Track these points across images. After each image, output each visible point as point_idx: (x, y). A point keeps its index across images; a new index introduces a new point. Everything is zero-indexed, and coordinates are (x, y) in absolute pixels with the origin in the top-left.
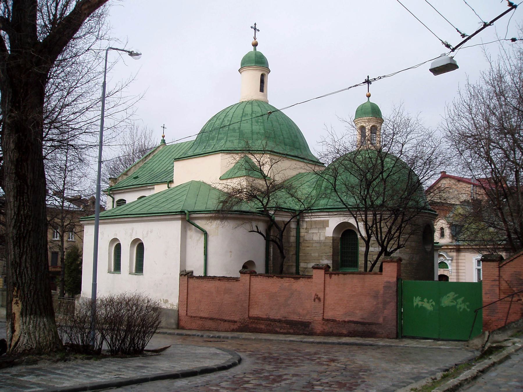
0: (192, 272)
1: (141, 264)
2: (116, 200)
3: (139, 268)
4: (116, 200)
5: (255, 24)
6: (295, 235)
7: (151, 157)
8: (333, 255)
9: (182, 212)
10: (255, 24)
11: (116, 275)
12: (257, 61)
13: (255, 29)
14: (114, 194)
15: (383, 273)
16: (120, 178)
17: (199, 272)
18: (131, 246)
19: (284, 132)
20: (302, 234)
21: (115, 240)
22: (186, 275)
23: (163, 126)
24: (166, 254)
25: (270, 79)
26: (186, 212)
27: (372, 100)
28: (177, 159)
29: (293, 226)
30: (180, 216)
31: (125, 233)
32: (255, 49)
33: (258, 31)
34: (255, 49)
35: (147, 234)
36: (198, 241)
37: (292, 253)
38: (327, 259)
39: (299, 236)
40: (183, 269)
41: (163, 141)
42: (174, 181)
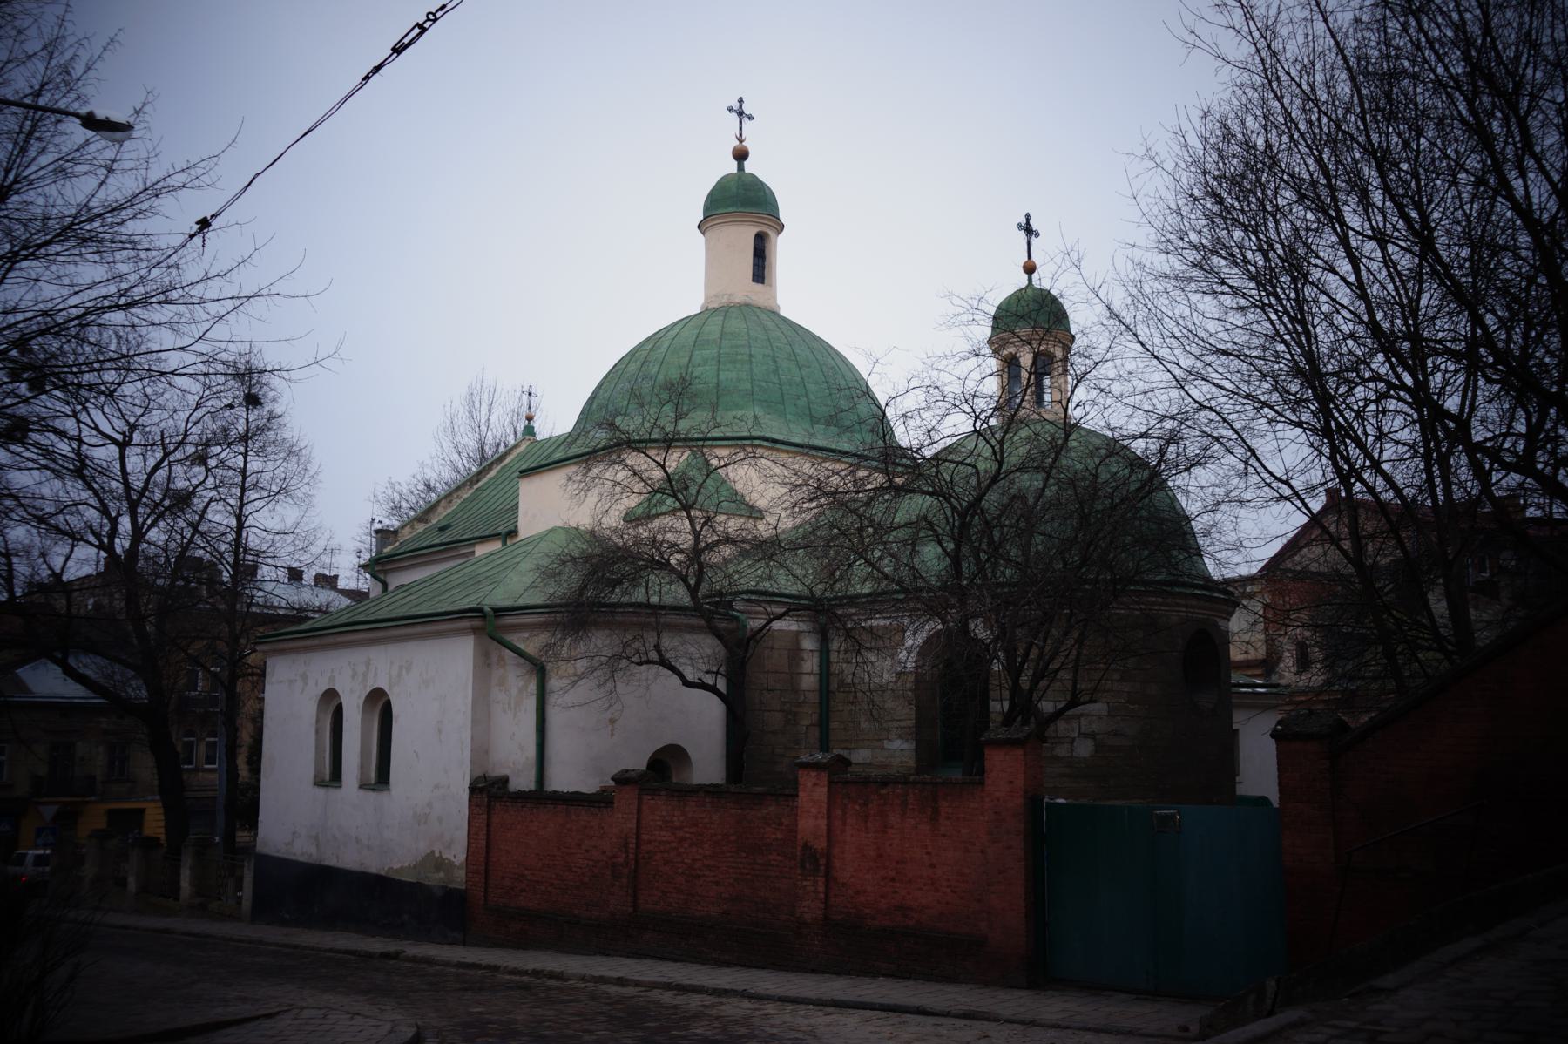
3: (383, 777)
5: (741, 101)
6: (816, 669)
7: (493, 473)
8: (917, 725)
10: (741, 101)
11: (333, 793)
13: (741, 114)
14: (386, 572)
15: (362, 792)
16: (407, 529)
17: (523, 781)
18: (364, 711)
19: (811, 387)
20: (835, 668)
22: (488, 792)
24: (440, 731)
25: (783, 249)
26: (487, 609)
27: (1042, 280)
28: (526, 473)
29: (808, 644)
30: (465, 624)
31: (351, 672)
32: (741, 168)
33: (750, 118)
34: (741, 168)
35: (399, 675)
37: (806, 722)
38: (900, 737)
39: (829, 674)
40: (479, 773)
41: (529, 430)
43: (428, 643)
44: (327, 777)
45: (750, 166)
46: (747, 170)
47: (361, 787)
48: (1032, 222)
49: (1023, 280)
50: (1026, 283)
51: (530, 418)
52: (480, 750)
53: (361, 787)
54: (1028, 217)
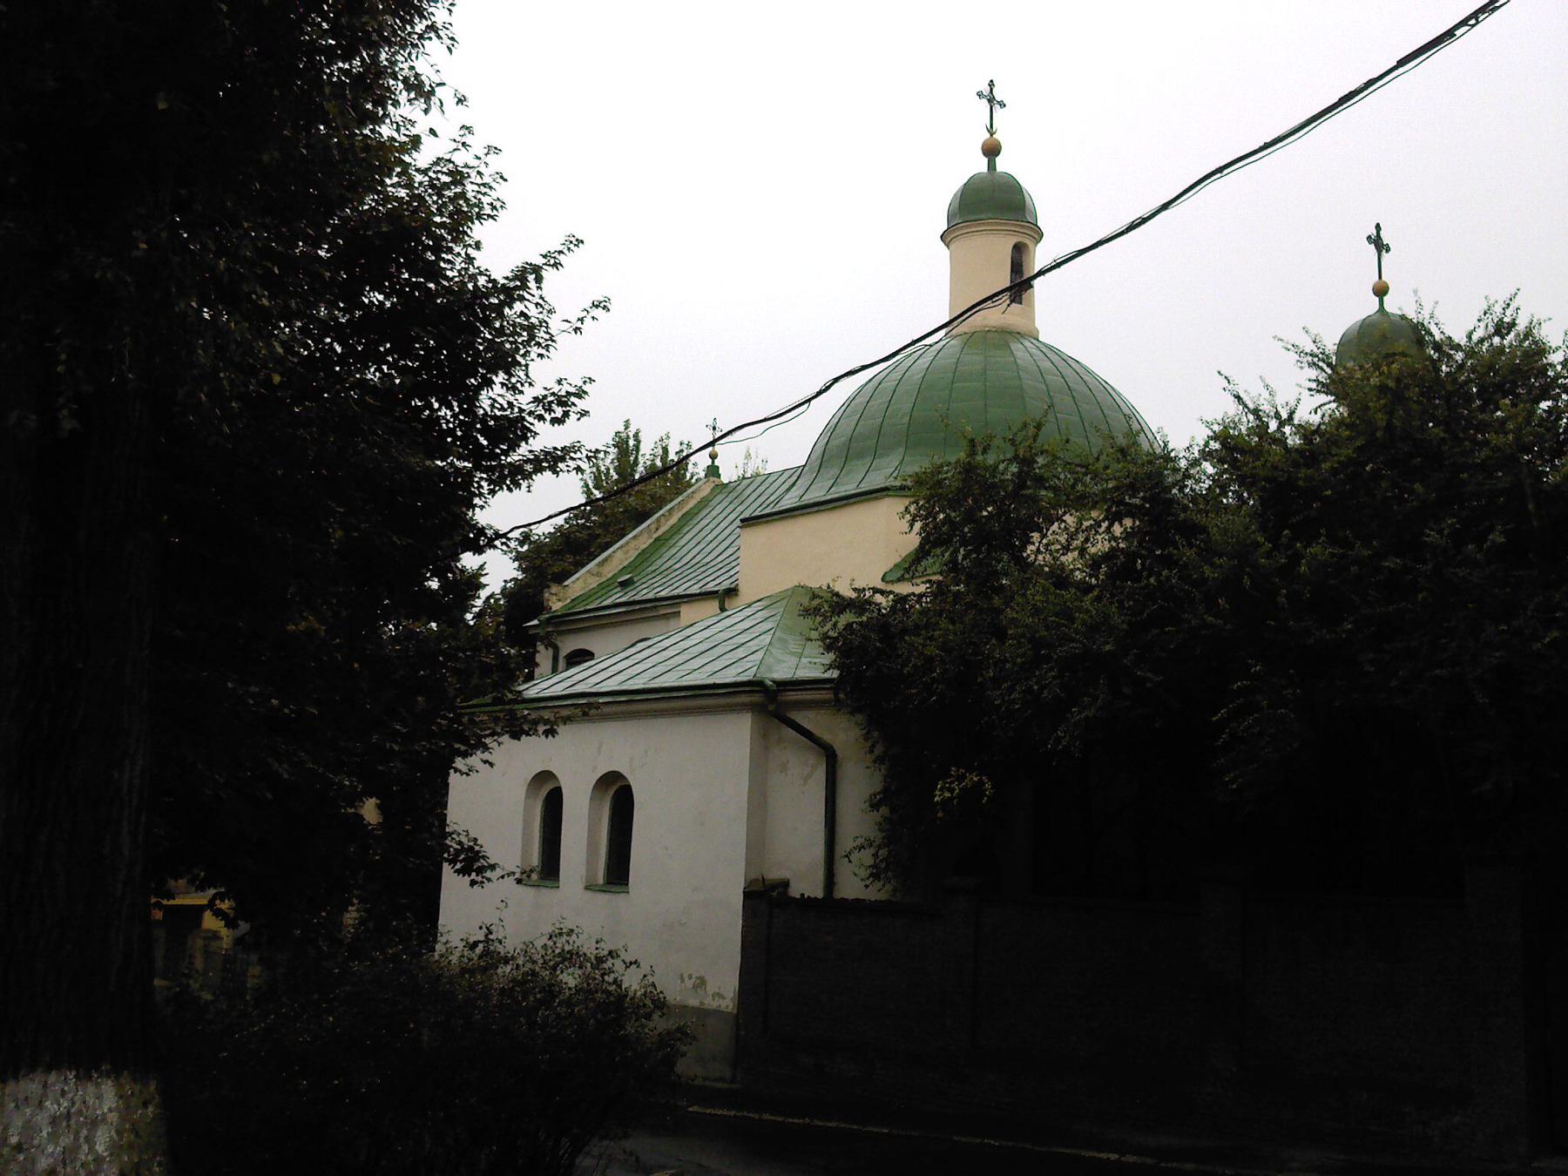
0: (785, 884)
1: (635, 844)
2: (563, 653)
3: (617, 872)
4: (563, 653)
9: (755, 685)
11: (546, 895)
12: (991, 206)
13: (991, 100)
15: (589, 894)
17: (808, 885)
18: (527, 797)
21: (545, 776)
23: (711, 423)
31: (577, 757)
32: (992, 166)
33: (1002, 105)
34: (992, 166)
36: (806, 779)
42: (741, 588)
43: (678, 719)
44: (601, 881)
45: (1002, 164)
46: (999, 169)
47: (587, 888)
48: (1382, 233)
49: (1370, 306)
50: (1377, 307)
51: (1415, 292)
52: (757, 845)
53: (587, 888)
54: (1378, 227)
